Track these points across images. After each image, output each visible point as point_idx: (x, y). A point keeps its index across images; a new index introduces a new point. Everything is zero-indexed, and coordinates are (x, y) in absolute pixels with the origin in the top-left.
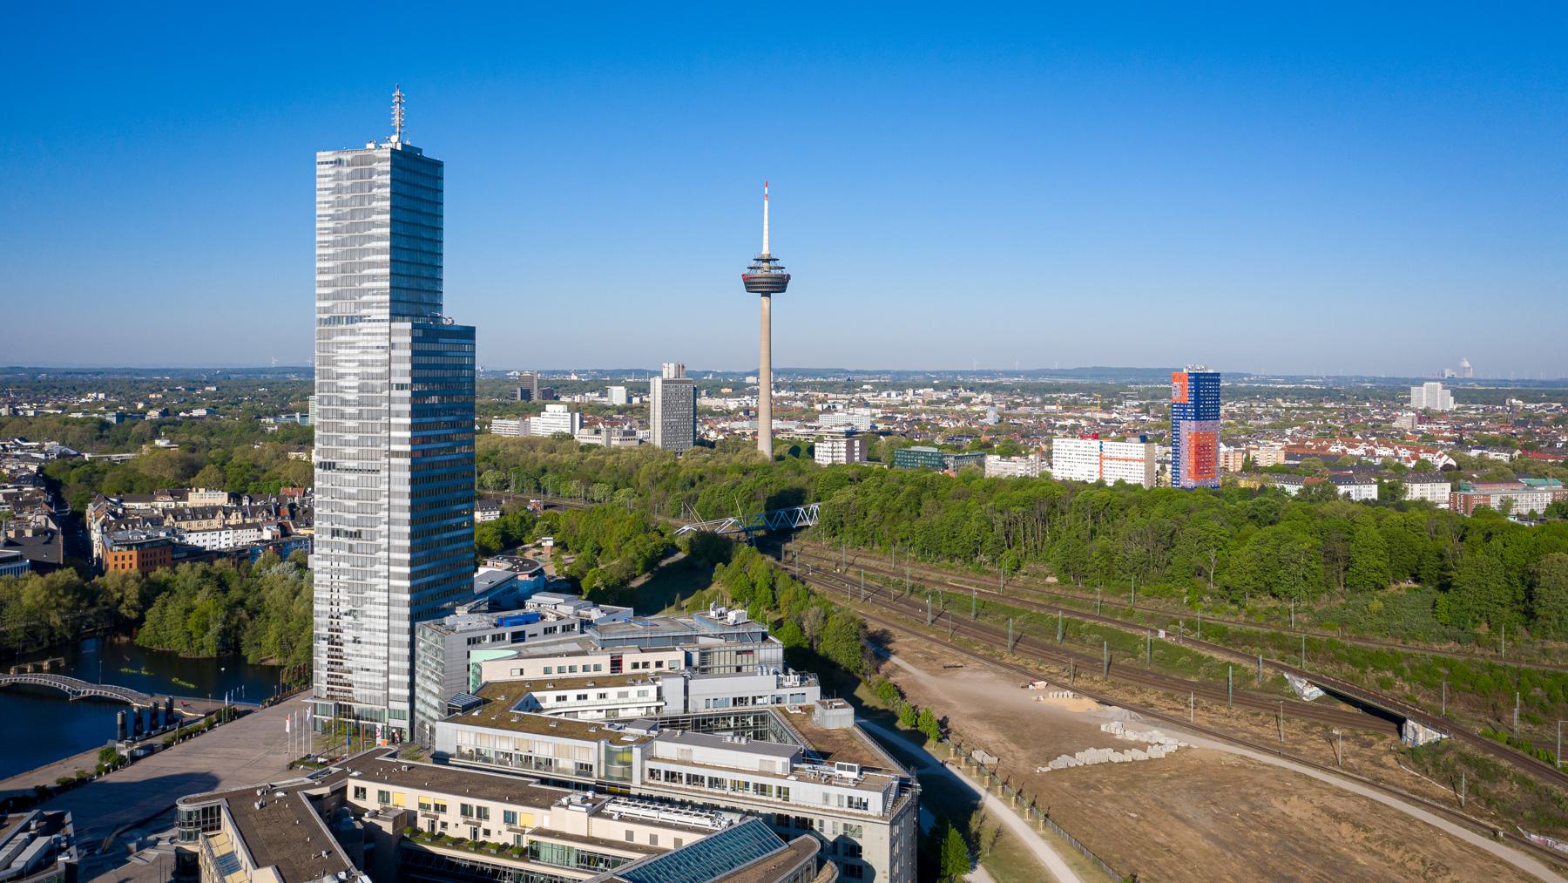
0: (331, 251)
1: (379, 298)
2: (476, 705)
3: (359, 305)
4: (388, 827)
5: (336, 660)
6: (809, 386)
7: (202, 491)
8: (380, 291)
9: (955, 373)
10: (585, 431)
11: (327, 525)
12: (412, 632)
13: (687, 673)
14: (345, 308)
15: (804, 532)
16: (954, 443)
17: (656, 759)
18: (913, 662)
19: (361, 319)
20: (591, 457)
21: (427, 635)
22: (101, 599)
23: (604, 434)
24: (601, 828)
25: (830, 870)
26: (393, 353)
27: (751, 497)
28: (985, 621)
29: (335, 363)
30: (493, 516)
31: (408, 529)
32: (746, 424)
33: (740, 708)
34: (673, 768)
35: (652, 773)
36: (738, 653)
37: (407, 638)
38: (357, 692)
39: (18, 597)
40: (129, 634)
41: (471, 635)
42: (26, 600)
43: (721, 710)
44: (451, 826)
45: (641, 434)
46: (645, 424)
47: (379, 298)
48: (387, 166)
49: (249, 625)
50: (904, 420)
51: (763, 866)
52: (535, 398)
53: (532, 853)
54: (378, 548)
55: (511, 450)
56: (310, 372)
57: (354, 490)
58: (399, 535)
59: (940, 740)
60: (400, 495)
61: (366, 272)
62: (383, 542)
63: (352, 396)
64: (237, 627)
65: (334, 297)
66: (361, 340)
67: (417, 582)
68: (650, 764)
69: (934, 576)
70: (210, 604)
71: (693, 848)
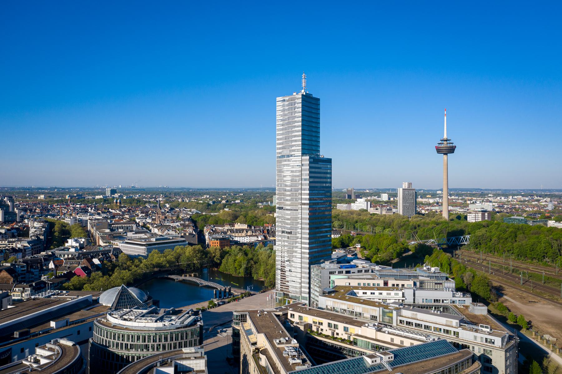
0: (281, 132)
1: (298, 148)
2: (333, 292)
3: (291, 151)
4: (302, 328)
5: (283, 277)
6: (463, 194)
7: (239, 224)
8: (298, 145)
9: (532, 190)
10: (372, 209)
11: (280, 229)
12: (310, 269)
13: (415, 288)
14: (286, 152)
15: (463, 246)
16: (532, 216)
17: (403, 316)
18: (514, 299)
19: (291, 156)
20: (375, 217)
21: (315, 269)
22: (209, 255)
23: (379, 210)
24: (381, 336)
25: (477, 365)
26: (303, 167)
27: (441, 232)
28: (549, 285)
29: (283, 172)
30: (338, 236)
31: (308, 231)
32: (437, 208)
33: (436, 304)
34: (409, 320)
35: (401, 321)
36: (436, 284)
37: (308, 271)
38: (291, 289)
39: (185, 253)
40: (217, 267)
41: (331, 271)
42: (187, 254)
43: (428, 304)
44: (324, 330)
45: (394, 210)
46: (396, 207)
47: (298, 148)
48: (300, 101)
49: (254, 266)
50: (508, 208)
51: (448, 358)
52: (353, 198)
53: (355, 343)
54: (297, 238)
55: (344, 214)
56: (274, 189)
57: (289, 217)
58: (305, 233)
59: (528, 329)
60: (305, 219)
61: (293, 139)
62: (299, 235)
63: (288, 183)
64: (251, 267)
65: (283, 148)
66: (291, 163)
67: (312, 251)
68: (400, 318)
69: (524, 266)
70: (242, 258)
71: (418, 346)
